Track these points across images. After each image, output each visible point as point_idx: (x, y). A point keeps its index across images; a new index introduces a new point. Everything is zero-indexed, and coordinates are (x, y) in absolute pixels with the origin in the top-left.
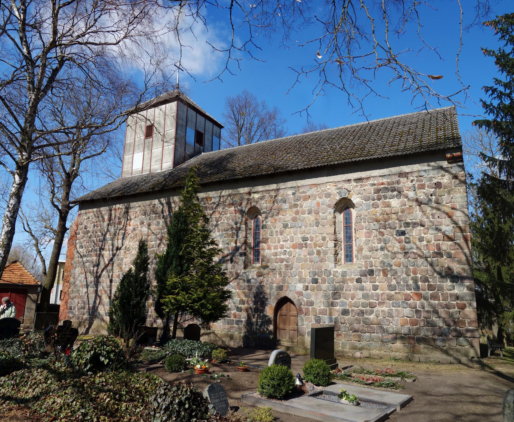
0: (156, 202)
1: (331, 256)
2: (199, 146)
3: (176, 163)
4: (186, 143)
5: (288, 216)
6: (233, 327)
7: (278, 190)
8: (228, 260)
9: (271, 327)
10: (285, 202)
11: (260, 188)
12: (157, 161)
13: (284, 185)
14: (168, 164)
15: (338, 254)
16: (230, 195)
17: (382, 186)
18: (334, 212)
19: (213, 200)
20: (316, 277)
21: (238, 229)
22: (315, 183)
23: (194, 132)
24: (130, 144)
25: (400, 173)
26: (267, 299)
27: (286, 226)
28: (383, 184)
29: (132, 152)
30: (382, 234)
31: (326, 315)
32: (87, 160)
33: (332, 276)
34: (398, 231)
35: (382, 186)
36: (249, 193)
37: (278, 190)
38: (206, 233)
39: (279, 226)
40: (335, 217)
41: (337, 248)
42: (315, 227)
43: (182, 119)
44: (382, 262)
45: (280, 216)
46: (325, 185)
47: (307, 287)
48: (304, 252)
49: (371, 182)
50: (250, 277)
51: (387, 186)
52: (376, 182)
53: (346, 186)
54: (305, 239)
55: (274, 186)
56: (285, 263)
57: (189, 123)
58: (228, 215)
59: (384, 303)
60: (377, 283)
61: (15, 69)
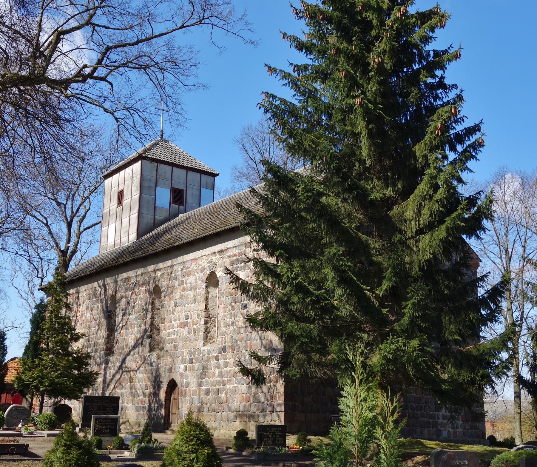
0: (95, 284)
1: (201, 335)
2: (177, 206)
3: (139, 235)
4: (155, 207)
5: (177, 295)
6: (140, 414)
7: (172, 266)
8: (139, 344)
9: (163, 411)
10: (176, 279)
11: (161, 265)
12: (125, 232)
13: (176, 261)
14: (133, 237)
15: (210, 331)
16: (142, 274)
17: (235, 258)
18: (207, 287)
19: (132, 280)
20: (192, 357)
21: (147, 310)
22: (194, 258)
23: (66, 224)
24: (107, 213)
25: (245, 244)
26: (162, 382)
27: (176, 305)
28: (235, 255)
29: (107, 224)
30: (233, 307)
31: (196, 395)
32: (87, 230)
33: (201, 355)
34: (242, 304)
35: (235, 258)
36: (155, 271)
37: (172, 266)
38: (458, 320)
39: (172, 303)
40: (207, 293)
41: (209, 325)
42: (194, 304)
43: (150, 180)
44: (232, 338)
45: (174, 294)
46: (200, 259)
47: (186, 367)
48: (185, 331)
49: (230, 253)
50: (152, 361)
51: (238, 257)
52: (231, 254)
53: (214, 259)
54: (187, 317)
55: (169, 263)
56: (174, 343)
57: (161, 181)
58: (141, 295)
59: (230, 380)
60: (228, 360)
61: (96, 74)
